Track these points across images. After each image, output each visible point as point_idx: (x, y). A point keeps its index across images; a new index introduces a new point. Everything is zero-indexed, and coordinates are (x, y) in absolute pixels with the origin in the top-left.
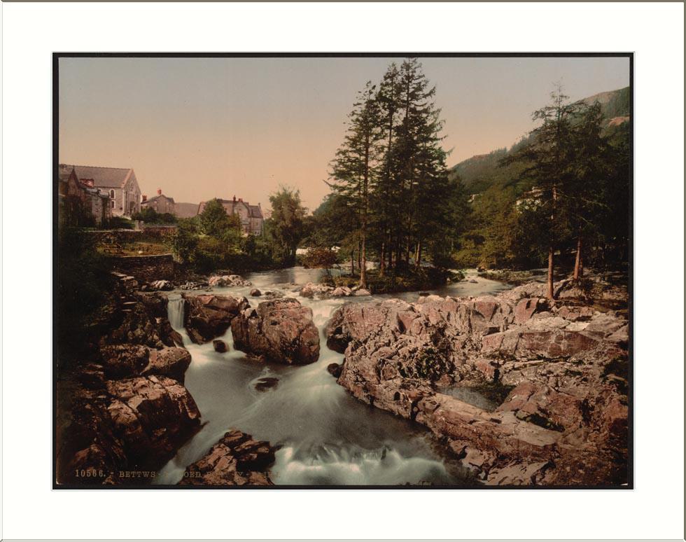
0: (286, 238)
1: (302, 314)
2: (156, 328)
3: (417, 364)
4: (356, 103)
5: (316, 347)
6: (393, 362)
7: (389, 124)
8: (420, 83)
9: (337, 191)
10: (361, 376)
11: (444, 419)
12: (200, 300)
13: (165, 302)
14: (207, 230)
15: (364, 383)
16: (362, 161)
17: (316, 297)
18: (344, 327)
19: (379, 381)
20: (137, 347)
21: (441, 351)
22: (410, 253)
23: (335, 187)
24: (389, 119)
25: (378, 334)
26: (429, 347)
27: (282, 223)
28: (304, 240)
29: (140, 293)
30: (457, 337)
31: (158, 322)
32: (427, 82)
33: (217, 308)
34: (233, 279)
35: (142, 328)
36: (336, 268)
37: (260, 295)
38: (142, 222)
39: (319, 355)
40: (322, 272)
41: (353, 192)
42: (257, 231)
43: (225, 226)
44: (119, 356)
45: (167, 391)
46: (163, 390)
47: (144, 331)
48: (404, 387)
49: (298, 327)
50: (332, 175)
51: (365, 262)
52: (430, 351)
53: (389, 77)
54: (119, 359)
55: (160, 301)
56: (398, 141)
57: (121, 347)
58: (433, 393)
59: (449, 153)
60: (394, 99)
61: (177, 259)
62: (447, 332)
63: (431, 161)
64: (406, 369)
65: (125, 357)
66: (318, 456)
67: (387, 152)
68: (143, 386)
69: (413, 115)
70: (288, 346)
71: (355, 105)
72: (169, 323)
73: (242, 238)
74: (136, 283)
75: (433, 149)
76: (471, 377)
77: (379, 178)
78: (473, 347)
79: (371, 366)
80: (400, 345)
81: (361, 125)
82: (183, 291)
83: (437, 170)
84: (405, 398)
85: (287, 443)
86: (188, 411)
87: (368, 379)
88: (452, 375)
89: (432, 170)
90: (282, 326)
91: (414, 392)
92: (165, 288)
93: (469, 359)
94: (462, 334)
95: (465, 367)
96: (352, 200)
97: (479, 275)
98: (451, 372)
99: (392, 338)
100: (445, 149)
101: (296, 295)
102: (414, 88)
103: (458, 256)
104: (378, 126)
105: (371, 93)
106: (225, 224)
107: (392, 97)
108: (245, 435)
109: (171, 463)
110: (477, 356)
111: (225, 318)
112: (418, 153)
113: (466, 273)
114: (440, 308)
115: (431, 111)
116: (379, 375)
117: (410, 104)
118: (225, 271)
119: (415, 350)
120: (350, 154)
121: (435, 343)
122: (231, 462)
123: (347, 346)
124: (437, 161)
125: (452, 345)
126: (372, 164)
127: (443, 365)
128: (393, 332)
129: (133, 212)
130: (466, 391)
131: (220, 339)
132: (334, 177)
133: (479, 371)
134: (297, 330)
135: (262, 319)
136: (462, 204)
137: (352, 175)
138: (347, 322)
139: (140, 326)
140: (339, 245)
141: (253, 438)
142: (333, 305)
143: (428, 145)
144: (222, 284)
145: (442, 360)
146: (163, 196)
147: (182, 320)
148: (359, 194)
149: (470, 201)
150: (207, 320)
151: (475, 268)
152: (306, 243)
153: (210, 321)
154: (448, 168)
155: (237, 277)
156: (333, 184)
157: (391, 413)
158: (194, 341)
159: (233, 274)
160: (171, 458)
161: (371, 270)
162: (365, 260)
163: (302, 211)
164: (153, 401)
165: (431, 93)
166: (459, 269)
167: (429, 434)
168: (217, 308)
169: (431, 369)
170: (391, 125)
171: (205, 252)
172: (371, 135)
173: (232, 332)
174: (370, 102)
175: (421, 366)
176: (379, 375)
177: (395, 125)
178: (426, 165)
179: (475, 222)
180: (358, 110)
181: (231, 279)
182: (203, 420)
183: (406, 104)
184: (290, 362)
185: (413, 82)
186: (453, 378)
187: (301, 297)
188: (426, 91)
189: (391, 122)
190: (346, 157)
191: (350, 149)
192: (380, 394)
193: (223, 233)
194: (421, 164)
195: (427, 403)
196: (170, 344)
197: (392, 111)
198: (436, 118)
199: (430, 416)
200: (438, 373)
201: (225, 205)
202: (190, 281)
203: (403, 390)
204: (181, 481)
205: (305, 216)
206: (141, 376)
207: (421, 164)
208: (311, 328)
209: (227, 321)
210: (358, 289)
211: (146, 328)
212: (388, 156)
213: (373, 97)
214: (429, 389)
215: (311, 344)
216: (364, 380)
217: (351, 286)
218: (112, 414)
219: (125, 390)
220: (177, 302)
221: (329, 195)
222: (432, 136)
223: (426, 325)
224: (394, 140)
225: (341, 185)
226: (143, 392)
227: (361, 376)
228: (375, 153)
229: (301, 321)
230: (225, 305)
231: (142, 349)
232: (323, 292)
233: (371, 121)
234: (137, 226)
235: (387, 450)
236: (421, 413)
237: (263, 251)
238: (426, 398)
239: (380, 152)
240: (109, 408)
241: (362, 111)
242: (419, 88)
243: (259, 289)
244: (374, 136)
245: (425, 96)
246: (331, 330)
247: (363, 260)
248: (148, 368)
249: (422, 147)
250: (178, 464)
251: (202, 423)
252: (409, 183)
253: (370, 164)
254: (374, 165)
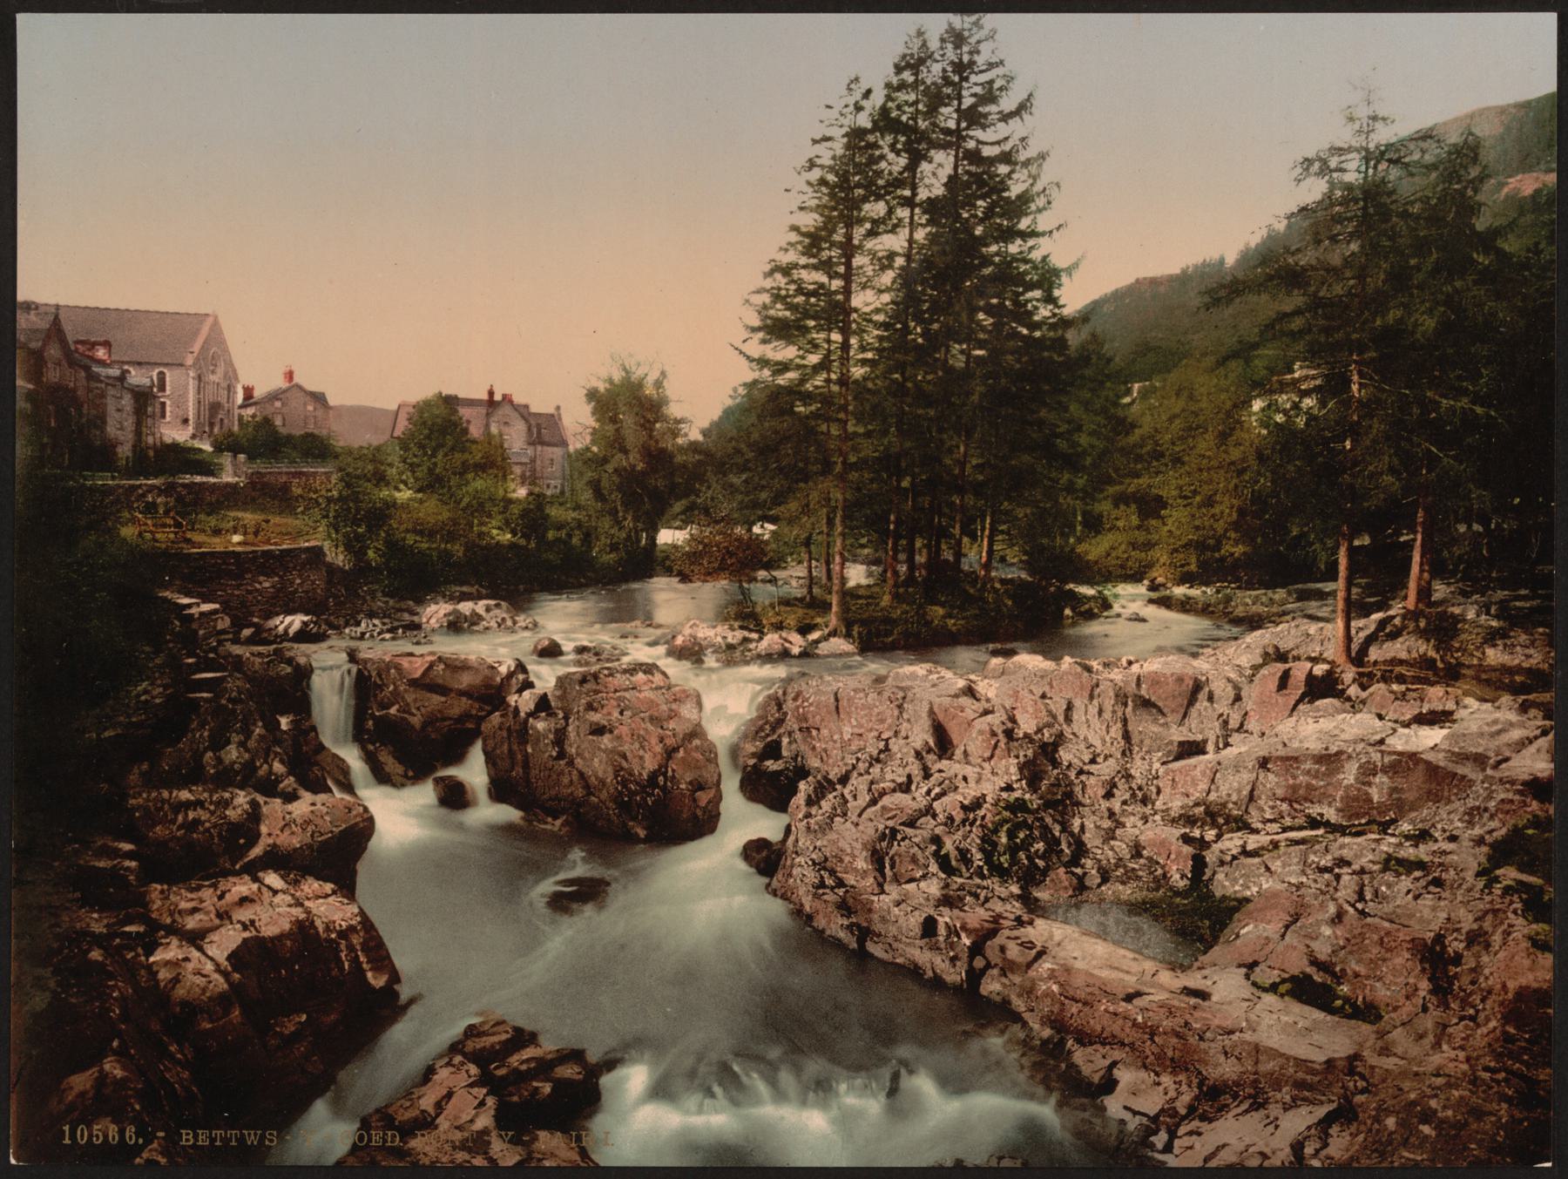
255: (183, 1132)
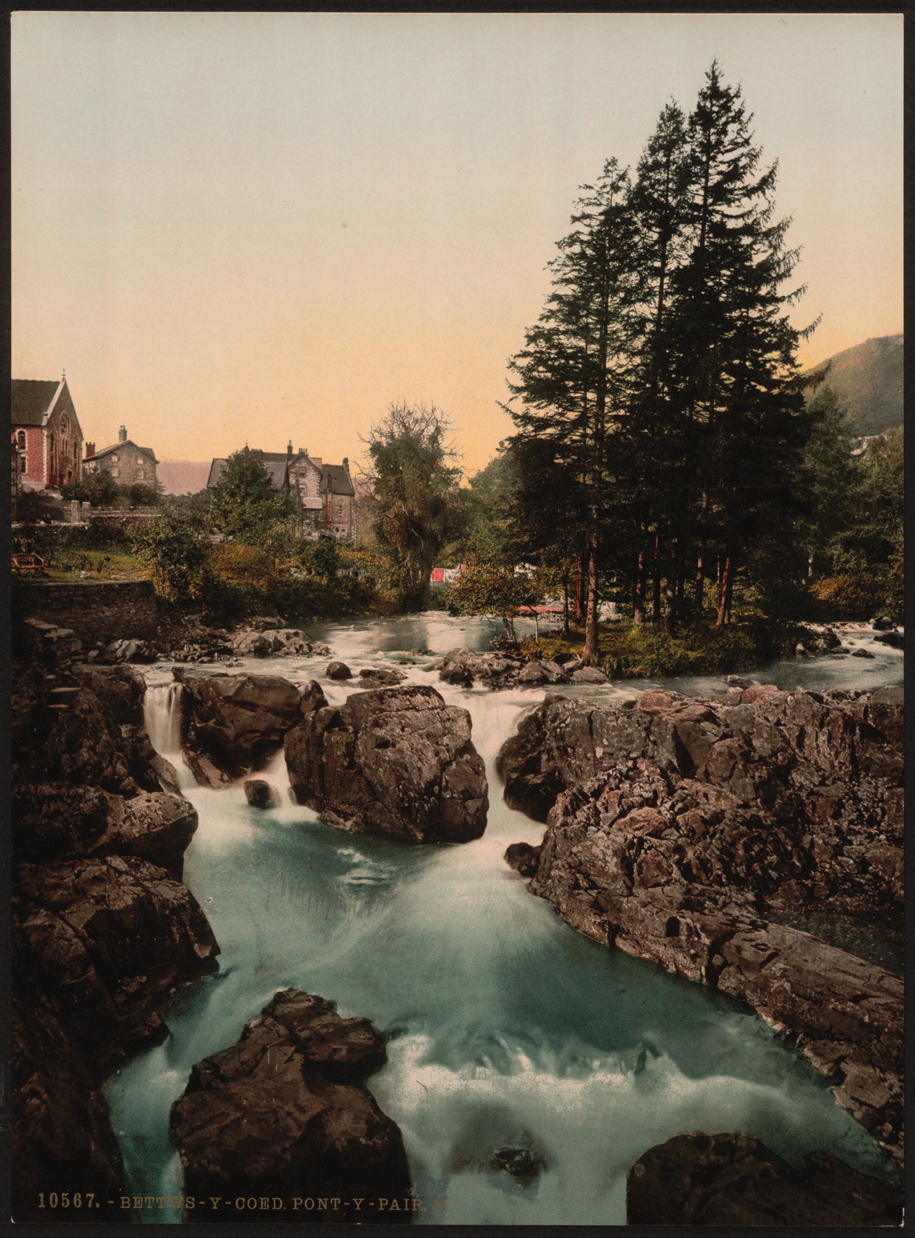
0: (410, 542)
1: (448, 724)
2: (120, 748)
3: (721, 851)
4: (578, 214)
5: (479, 803)
6: (663, 845)
7: (657, 264)
8: (737, 160)
9: (530, 428)
10: (587, 876)
11: (787, 986)
12: (215, 686)
13: (138, 690)
14: (228, 524)
15: (594, 893)
16: (592, 355)
17: (478, 686)
18: (544, 757)
19: (629, 889)
20: (81, 791)
21: (780, 822)
22: (707, 581)
23: (526, 419)
24: (661, 251)
25: (627, 777)
26: (753, 811)
27: (400, 507)
28: (449, 549)
29: (86, 669)
30: (822, 790)
31: (124, 735)
32: (753, 157)
33: (252, 706)
34: (288, 638)
35: (92, 748)
36: (525, 615)
37: (350, 676)
38: (86, 504)
39: (486, 821)
40: (491, 624)
41: (571, 431)
42: (341, 526)
43: (269, 514)
44: (44, 808)
45: (145, 889)
46: (140, 888)
47: (96, 754)
48: (690, 904)
49: (437, 754)
50: (519, 390)
51: (596, 604)
52: (754, 822)
53: (661, 147)
54: (44, 817)
55: (127, 686)
56: (679, 305)
57: (47, 789)
58: (759, 922)
59: (805, 333)
60: (672, 201)
61: (163, 589)
62: (797, 778)
63: (761, 355)
64: (694, 862)
65: (58, 812)
66: (486, 1059)
67: (651, 332)
68: (97, 880)
69: (717, 240)
70: (415, 799)
71: (575, 219)
72: (147, 737)
73: (306, 543)
74: (77, 646)
75: (765, 324)
76: (857, 889)
77: (632, 397)
78: (861, 816)
79: (610, 852)
80: (680, 805)
81: (590, 268)
82: (179, 665)
83: (775, 377)
84: (691, 931)
85: (413, 1024)
86: (192, 938)
87: (602, 882)
88: (808, 883)
89: (764, 376)
90: (401, 751)
91: (715, 920)
92: (140, 658)
93: (850, 842)
94: (834, 782)
95: (839, 864)
96: (565, 451)
97: (877, 639)
98: (805, 873)
99: (660, 786)
100: (796, 324)
101: (432, 679)
102: (720, 173)
103: (824, 590)
104: (632, 269)
105: (615, 188)
106: (269, 509)
107: (666, 197)
108: (318, 1000)
109: (158, 1056)
110: (871, 837)
111: (270, 730)
112: (730, 335)
113: (845, 633)
114: (781, 716)
115: (765, 226)
116: (629, 874)
117: (711, 213)
118: (268, 619)
119: (718, 817)
120: (564, 339)
121: (768, 803)
122: (290, 1059)
123: (553, 802)
124: (776, 354)
125: (809, 809)
126: (616, 362)
127: (785, 857)
128: (663, 774)
129: (65, 481)
130: (846, 922)
131: (260, 777)
132: (525, 394)
133: (875, 875)
134: (434, 761)
135: (356, 732)
136: (836, 460)
137: (566, 390)
138: (554, 745)
139: (87, 743)
140: (533, 561)
141: (546, 1182)
142: (521, 705)
143: (754, 314)
144: (262, 651)
145: (784, 845)
146: (130, 444)
147: (177, 728)
148: (584, 436)
149: (857, 452)
150: (230, 732)
151: (867, 620)
152: (453, 554)
153: (238, 736)
154: (801, 370)
155: (296, 634)
156: (520, 413)
157: (658, 966)
158: (201, 779)
159: (287, 627)
160: (159, 1043)
161: (609, 621)
162: (597, 597)
163: (447, 476)
164: (119, 912)
165: (766, 183)
166: (828, 622)
167: (751, 1019)
168: (252, 706)
169: (756, 866)
170: (664, 265)
171: (224, 576)
172: (615, 292)
173: (287, 760)
174: (612, 213)
175: (732, 856)
176: (629, 874)
177: (672, 265)
178: (748, 363)
179: (868, 506)
180: (584, 230)
181: (283, 640)
182: (223, 962)
183: (700, 215)
184: (420, 836)
185: (720, 157)
186: (811, 890)
187: (444, 684)
188: (751, 179)
189: (664, 259)
190: (553, 346)
191: (562, 328)
192: (632, 919)
193: (264, 529)
194: (736, 362)
195: (747, 945)
196: (152, 787)
197: (667, 232)
198: (776, 248)
199: (752, 977)
200: (774, 874)
201: (268, 465)
202: (192, 641)
203: (687, 913)
204: (183, 1096)
205: (451, 489)
206: (89, 857)
207: (736, 362)
208: (467, 757)
209: (275, 738)
210: (580, 667)
211: (99, 748)
212: (656, 343)
213: (619, 199)
214: (747, 915)
215: (468, 795)
216: (593, 886)
217: (561, 659)
218: (32, 938)
219: (57, 886)
220: (165, 691)
221: (510, 439)
222: (764, 290)
223: (746, 757)
224: (668, 303)
225: (541, 413)
226: (96, 890)
227: (587, 876)
228: (622, 335)
229: (446, 740)
230: (272, 698)
231: (92, 793)
232: (496, 674)
233: (614, 258)
234: (76, 514)
235: (648, 1053)
236: (732, 969)
237: (356, 574)
238: (743, 935)
239: (636, 334)
240: (25, 925)
241: (591, 233)
242: (735, 173)
243: (347, 663)
244: (622, 295)
245: (749, 192)
246: (515, 764)
247: (591, 596)
248: (105, 838)
249: (739, 319)
250: (173, 1060)
251: (223, 967)
252: (706, 409)
253: (610, 364)
254: (621, 366)
255: (123, 1198)
